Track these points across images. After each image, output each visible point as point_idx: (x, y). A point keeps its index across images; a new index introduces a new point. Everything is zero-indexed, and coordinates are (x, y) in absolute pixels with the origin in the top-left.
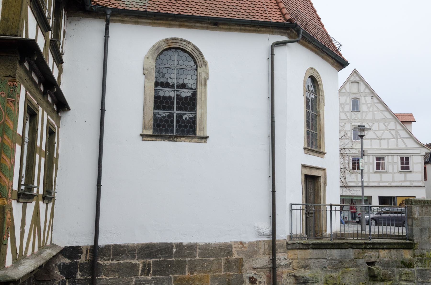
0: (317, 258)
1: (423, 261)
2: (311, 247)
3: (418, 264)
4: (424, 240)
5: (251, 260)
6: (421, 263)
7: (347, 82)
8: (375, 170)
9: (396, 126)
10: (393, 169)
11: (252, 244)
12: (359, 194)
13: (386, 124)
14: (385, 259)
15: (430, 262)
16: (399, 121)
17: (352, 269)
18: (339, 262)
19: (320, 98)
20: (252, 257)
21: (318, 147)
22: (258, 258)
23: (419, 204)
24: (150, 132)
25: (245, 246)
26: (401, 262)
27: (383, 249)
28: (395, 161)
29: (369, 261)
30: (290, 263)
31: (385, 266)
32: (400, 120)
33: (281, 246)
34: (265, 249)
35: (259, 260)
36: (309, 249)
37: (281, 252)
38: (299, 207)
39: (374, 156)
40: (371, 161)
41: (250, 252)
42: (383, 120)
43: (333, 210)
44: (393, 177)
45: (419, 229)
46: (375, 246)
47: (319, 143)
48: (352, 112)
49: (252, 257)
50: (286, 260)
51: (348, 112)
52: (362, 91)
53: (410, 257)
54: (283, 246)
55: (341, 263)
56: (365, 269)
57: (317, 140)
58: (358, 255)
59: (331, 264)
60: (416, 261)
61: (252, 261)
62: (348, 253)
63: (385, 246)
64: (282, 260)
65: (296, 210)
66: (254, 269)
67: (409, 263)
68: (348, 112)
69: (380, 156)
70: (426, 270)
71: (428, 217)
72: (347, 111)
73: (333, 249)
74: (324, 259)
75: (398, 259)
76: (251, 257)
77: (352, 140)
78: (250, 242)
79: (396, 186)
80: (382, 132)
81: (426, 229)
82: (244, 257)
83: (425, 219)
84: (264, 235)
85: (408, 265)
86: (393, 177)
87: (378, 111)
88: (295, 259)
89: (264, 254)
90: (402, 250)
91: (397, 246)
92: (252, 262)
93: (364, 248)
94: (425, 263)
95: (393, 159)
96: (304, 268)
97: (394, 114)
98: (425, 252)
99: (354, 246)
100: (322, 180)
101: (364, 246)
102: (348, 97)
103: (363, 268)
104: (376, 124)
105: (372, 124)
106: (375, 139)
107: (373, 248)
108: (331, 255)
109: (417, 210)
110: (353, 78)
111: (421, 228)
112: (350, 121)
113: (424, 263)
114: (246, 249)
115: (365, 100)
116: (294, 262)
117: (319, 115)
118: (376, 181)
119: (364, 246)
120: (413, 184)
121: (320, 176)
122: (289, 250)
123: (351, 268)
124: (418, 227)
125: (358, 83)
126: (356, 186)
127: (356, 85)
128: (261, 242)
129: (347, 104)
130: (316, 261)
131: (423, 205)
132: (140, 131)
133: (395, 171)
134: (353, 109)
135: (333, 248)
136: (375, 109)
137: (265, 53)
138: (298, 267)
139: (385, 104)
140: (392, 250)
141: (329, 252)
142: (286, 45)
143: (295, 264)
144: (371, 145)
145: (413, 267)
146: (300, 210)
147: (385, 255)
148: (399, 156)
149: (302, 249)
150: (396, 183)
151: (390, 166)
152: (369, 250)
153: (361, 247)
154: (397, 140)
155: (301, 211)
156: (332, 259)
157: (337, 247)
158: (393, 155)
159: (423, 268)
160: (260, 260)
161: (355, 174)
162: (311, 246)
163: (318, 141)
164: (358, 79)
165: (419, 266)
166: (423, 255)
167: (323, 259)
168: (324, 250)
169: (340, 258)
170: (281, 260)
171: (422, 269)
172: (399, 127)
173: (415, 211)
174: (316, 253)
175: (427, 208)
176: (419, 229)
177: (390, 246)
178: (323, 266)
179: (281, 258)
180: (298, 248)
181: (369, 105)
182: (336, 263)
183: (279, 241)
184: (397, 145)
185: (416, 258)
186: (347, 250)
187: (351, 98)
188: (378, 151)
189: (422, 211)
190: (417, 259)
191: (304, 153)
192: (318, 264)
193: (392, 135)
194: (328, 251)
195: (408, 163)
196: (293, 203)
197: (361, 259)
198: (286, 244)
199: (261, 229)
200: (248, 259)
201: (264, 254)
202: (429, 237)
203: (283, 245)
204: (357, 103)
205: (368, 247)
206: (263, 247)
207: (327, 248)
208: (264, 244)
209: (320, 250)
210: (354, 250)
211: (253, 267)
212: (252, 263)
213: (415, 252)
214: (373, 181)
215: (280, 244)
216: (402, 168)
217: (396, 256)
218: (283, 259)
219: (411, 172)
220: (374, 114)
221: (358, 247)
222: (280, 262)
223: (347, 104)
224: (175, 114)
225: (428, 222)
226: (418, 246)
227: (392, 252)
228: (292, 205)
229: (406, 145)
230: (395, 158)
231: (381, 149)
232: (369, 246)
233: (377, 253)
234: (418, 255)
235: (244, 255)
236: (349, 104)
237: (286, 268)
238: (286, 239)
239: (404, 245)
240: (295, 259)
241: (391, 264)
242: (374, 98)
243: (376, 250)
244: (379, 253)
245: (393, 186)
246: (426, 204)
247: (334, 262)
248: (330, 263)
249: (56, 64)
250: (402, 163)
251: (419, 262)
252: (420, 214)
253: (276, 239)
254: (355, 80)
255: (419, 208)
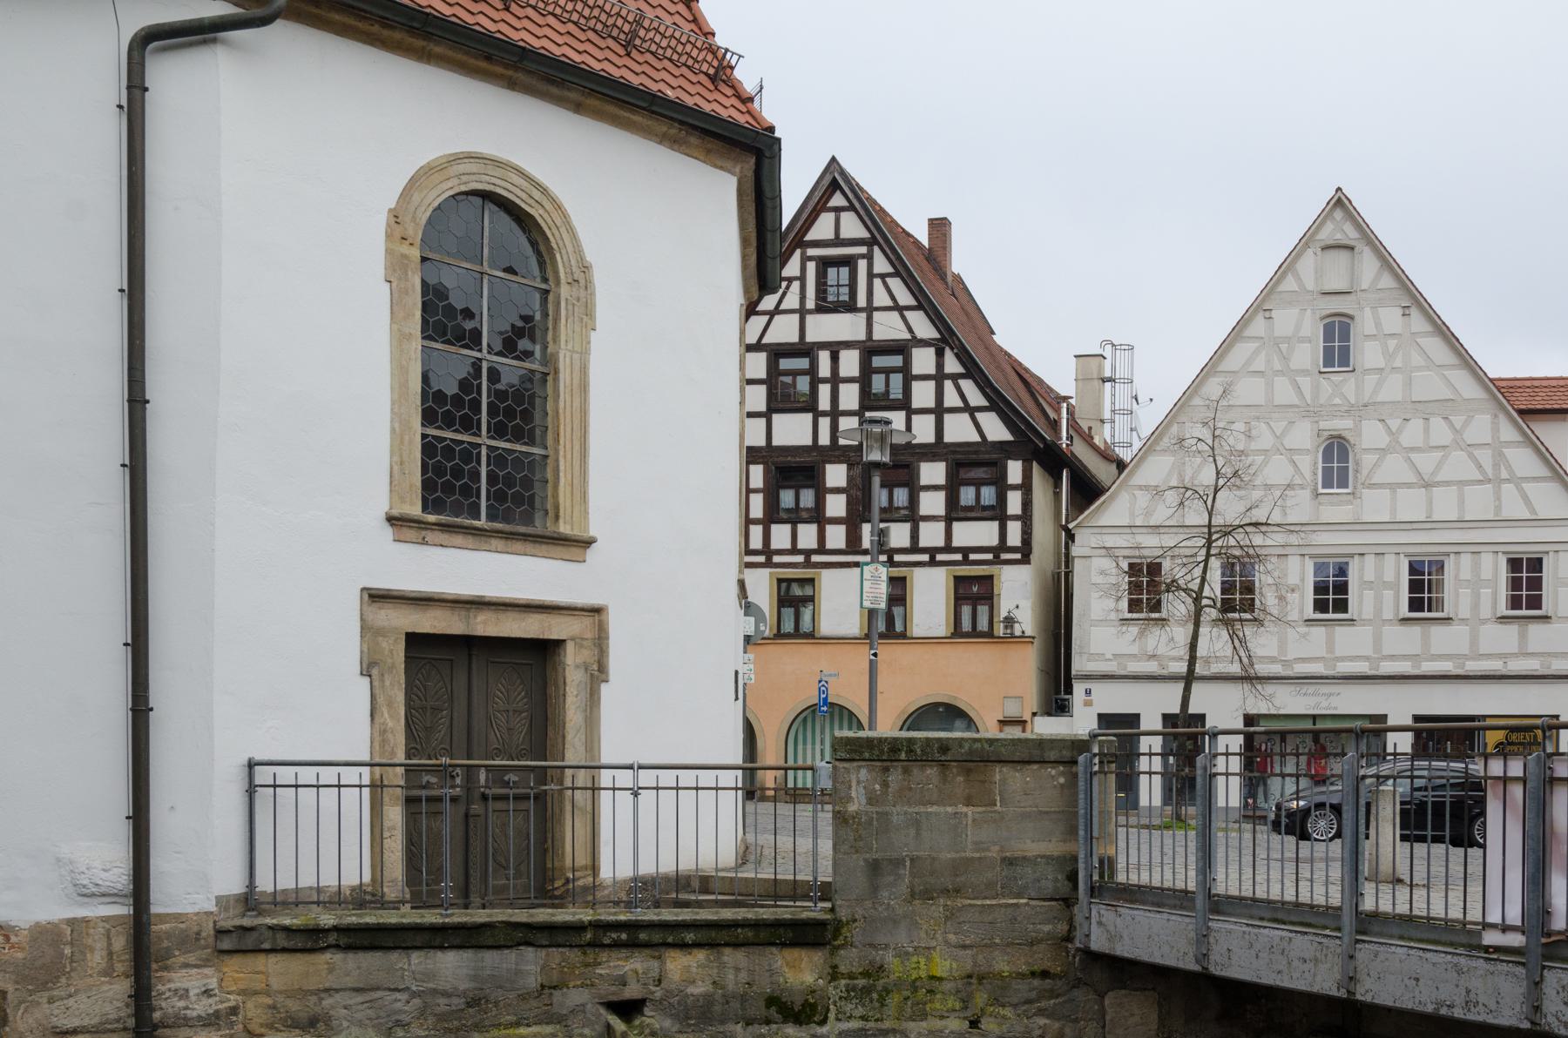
0: (361, 986)
1: (875, 996)
2: (334, 942)
3: (848, 1007)
4: (887, 909)
5: (45, 1000)
6: (863, 1006)
7: (1307, 245)
8: (1404, 611)
9: (1495, 430)
10: (1476, 606)
11: (46, 934)
12: (1336, 708)
13: (1458, 421)
14: (691, 990)
15: (907, 999)
16: (1510, 408)
17: (530, 1029)
18: (469, 1005)
19: (559, 295)
20: (50, 985)
21: (551, 514)
22: (77, 992)
23: (867, 755)
24: (415, 509)
25: (13, 939)
26: (766, 1000)
27: (683, 946)
28: (1486, 573)
29: (614, 998)
30: (234, 1011)
31: (690, 1018)
32: (1512, 405)
33: (189, 940)
34: (110, 954)
35: (82, 997)
36: (323, 950)
37: (186, 966)
38: (350, 775)
39: (1402, 556)
40: (1389, 576)
41: (39, 963)
42: (1445, 407)
43: (1505, 772)
44: (1474, 641)
45: (866, 860)
46: (643, 936)
47: (553, 496)
48: (1320, 372)
49: (50, 985)
50: (211, 996)
51: (1305, 372)
52: (1364, 287)
53: (811, 980)
54: (197, 940)
55: (479, 1005)
56: (594, 1030)
57: (547, 482)
58: (562, 972)
59: (429, 1011)
60: (841, 998)
61: (49, 1003)
62: (514, 966)
63: (690, 937)
64: (193, 999)
65: (275, 786)
66: (58, 1033)
67: (806, 1004)
68: (1305, 372)
69: (1425, 553)
70: (886, 1032)
71: (910, 810)
72: (1303, 371)
73: (441, 948)
74: (397, 990)
75: (755, 988)
76: (44, 986)
77: (1316, 489)
78: (37, 923)
79: (1483, 673)
80: (1438, 455)
81: (898, 863)
82: (10, 988)
83: (894, 819)
84: (104, 895)
85: (799, 1011)
86: (1474, 641)
87: (1428, 368)
88: (256, 993)
89: (108, 972)
90: (774, 949)
91: (750, 934)
92: (47, 1006)
93: (592, 944)
94: (883, 1005)
95: (1476, 568)
96: (303, 1029)
97: (1491, 380)
98: (890, 959)
99: (539, 935)
100: (572, 658)
101: (589, 936)
102: (1309, 311)
103: (583, 1027)
104: (1416, 424)
105: (1399, 421)
106: (1409, 485)
107: (633, 945)
108: (430, 975)
109: (858, 782)
110: (1329, 227)
111: (874, 860)
112: (1311, 412)
113: (877, 1005)
114: (20, 955)
115: (1378, 324)
116: (250, 1005)
117: (556, 372)
118: (1405, 657)
119: (589, 936)
120: (1554, 667)
121: (564, 641)
122: (226, 958)
123: (528, 1025)
124: (857, 852)
125: (1352, 248)
126: (1327, 678)
127: (1343, 255)
128: (92, 924)
129: (1302, 340)
130: (360, 998)
131: (891, 761)
132: (382, 503)
133: (1385, 617)
134: (1328, 361)
135: (437, 944)
136: (1417, 360)
137: (110, 87)
138: (271, 1026)
139: (1458, 340)
140: (727, 951)
141: (420, 963)
142: (214, 41)
143: (254, 1011)
144: (1394, 510)
145: (823, 1022)
146: (360, 786)
147: (694, 970)
148: (1504, 553)
149: (284, 950)
150: (1485, 663)
151: (1465, 593)
152: (615, 954)
153: (575, 940)
154: (1499, 487)
155: (366, 791)
156: (435, 992)
157: (457, 941)
158: (1476, 548)
159: (871, 1024)
160: (86, 1000)
161: (1323, 628)
162: (332, 939)
163: (550, 485)
164: (1350, 234)
165: (850, 1017)
166: (875, 971)
167: (390, 990)
168: (394, 956)
169: (472, 985)
170: (187, 997)
171: (863, 1029)
172: (1508, 432)
173: (850, 787)
174: (359, 968)
175: (906, 771)
176: (866, 860)
177: (713, 934)
178: (394, 1018)
179: (187, 991)
180: (266, 946)
181: (1392, 343)
182: (454, 1008)
183: (163, 918)
184: (1498, 508)
185: (843, 982)
186: (506, 951)
187: (1318, 316)
188: (1337, 534)
189: (885, 785)
190: (847, 986)
191: (392, 538)
192: (369, 1012)
193: (1480, 467)
194: (416, 957)
195: (1536, 584)
196: (258, 757)
197: (574, 991)
198: (212, 932)
199: (83, 869)
200: (31, 993)
201: (108, 972)
202: (913, 895)
203: (198, 933)
204: (1345, 336)
205: (607, 941)
206: (100, 945)
207: (409, 944)
208: (108, 931)
209: (378, 954)
210: (543, 953)
211: (53, 1027)
212: (48, 1011)
213: (837, 961)
214: (1392, 657)
215: (183, 931)
216: (1515, 603)
217: (743, 977)
218: (197, 991)
219: (1546, 618)
220: (1409, 383)
221: (560, 940)
222: (181, 1004)
223: (1303, 342)
224: (484, 451)
225: (912, 832)
226: (856, 933)
227: (725, 958)
228: (251, 765)
229: (1533, 511)
230: (1487, 560)
231: (1430, 524)
232: (614, 936)
233: (655, 964)
234: (854, 970)
235: (13, 977)
236: (1310, 342)
237: (211, 1028)
238: (214, 909)
239: (782, 931)
240: (256, 993)
241: (717, 1008)
242: (1415, 313)
243: (648, 951)
244: (663, 963)
245: (1471, 674)
246: (903, 756)
247: (442, 1001)
248: (426, 1006)
249: (781, 224)
250: (1515, 584)
251: (854, 1001)
252: (872, 800)
253: (154, 909)
254: (1339, 237)
255: (870, 771)
